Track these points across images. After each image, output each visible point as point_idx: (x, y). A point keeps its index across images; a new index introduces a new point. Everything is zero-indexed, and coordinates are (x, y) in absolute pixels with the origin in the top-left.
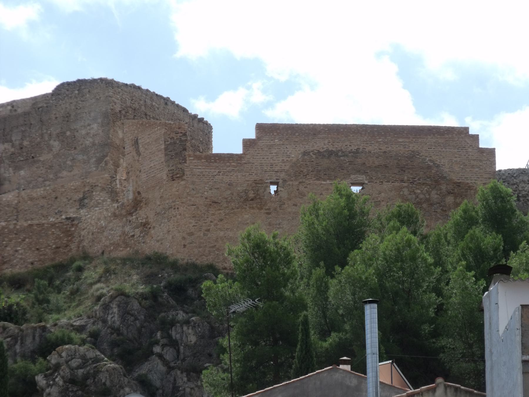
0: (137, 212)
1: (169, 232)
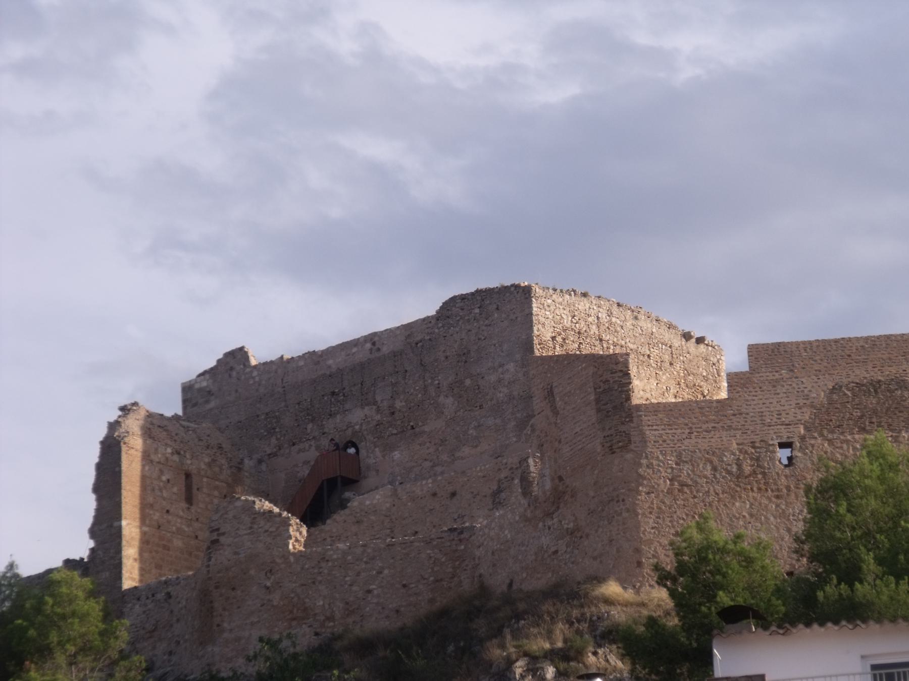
0: (560, 511)
1: (611, 541)
